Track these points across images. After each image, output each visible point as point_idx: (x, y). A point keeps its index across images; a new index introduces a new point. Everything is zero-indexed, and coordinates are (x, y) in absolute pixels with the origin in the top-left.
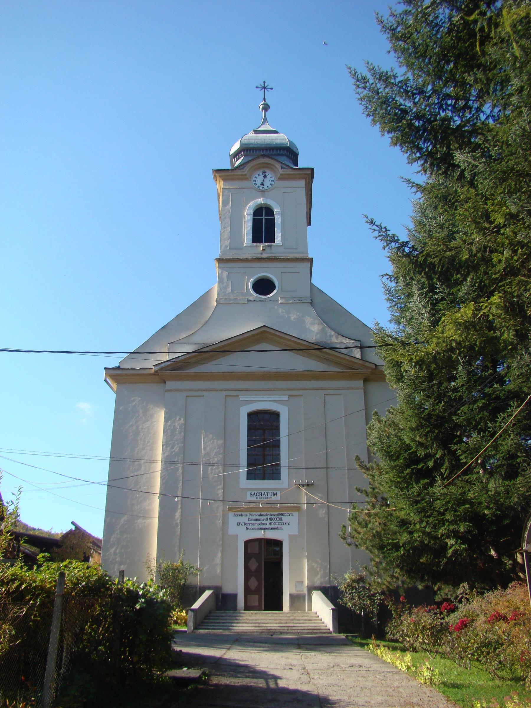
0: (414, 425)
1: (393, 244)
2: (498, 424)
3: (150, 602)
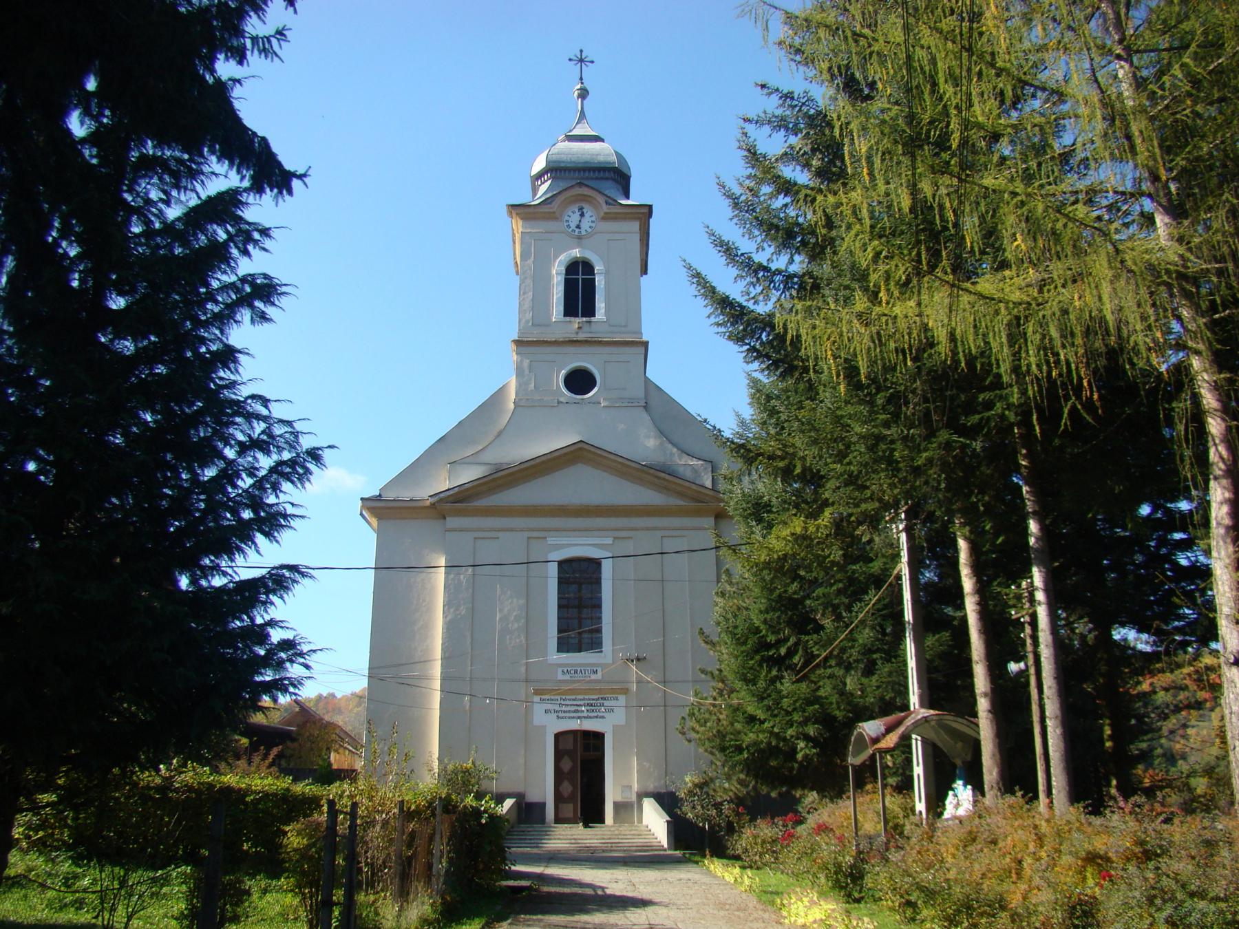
0: (763, 607)
2: (854, 614)
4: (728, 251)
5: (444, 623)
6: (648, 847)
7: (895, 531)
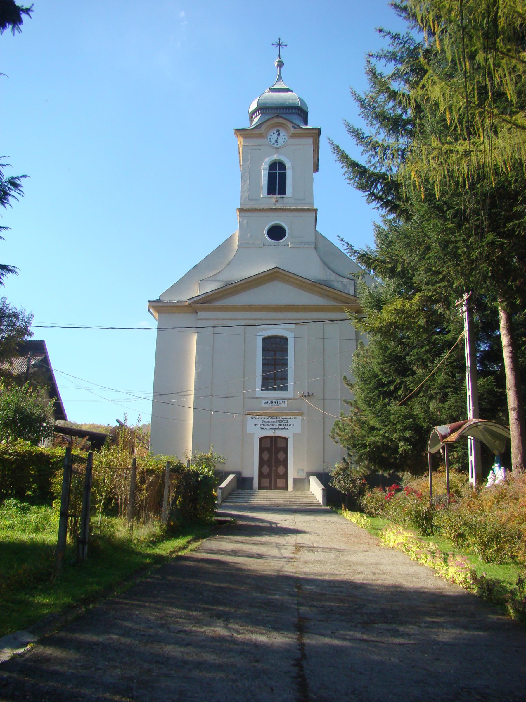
0: (380, 361)
1: (356, 254)
2: (435, 364)
3: (205, 477)
4: (357, 135)
5: (196, 373)
6: (313, 504)
7: (460, 312)
